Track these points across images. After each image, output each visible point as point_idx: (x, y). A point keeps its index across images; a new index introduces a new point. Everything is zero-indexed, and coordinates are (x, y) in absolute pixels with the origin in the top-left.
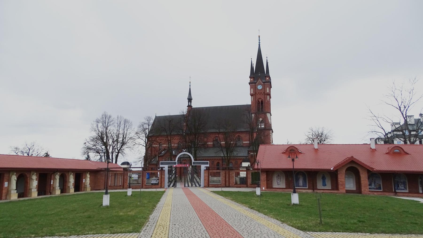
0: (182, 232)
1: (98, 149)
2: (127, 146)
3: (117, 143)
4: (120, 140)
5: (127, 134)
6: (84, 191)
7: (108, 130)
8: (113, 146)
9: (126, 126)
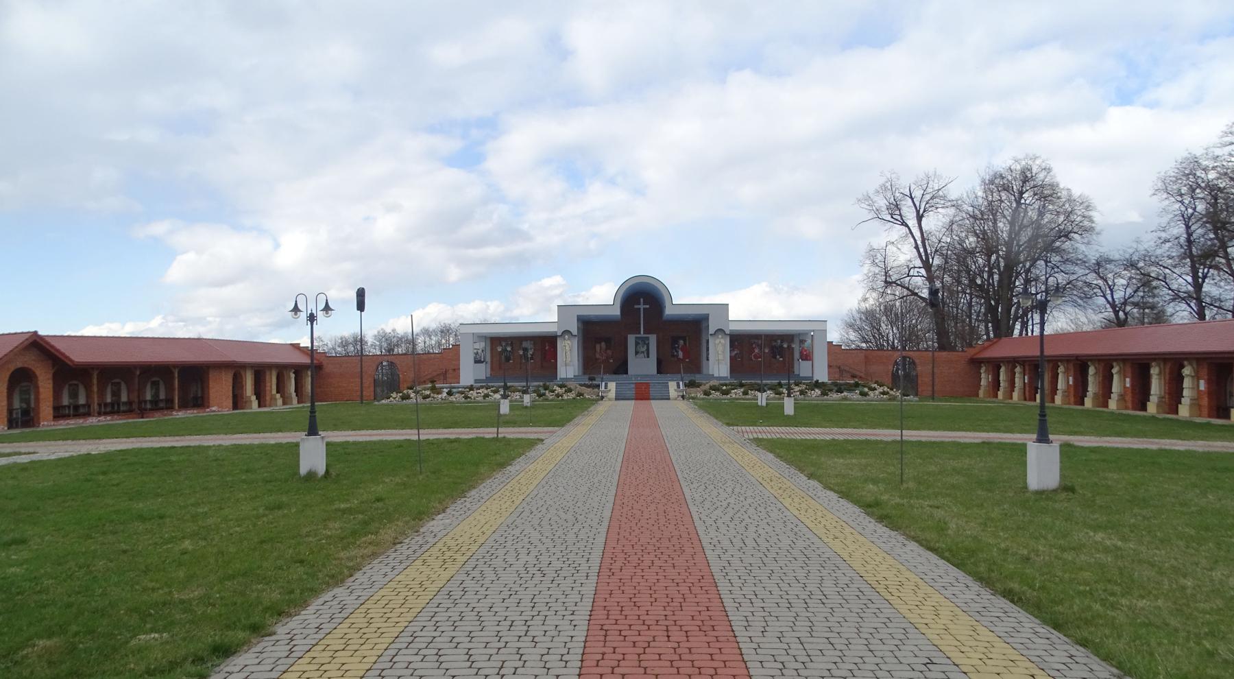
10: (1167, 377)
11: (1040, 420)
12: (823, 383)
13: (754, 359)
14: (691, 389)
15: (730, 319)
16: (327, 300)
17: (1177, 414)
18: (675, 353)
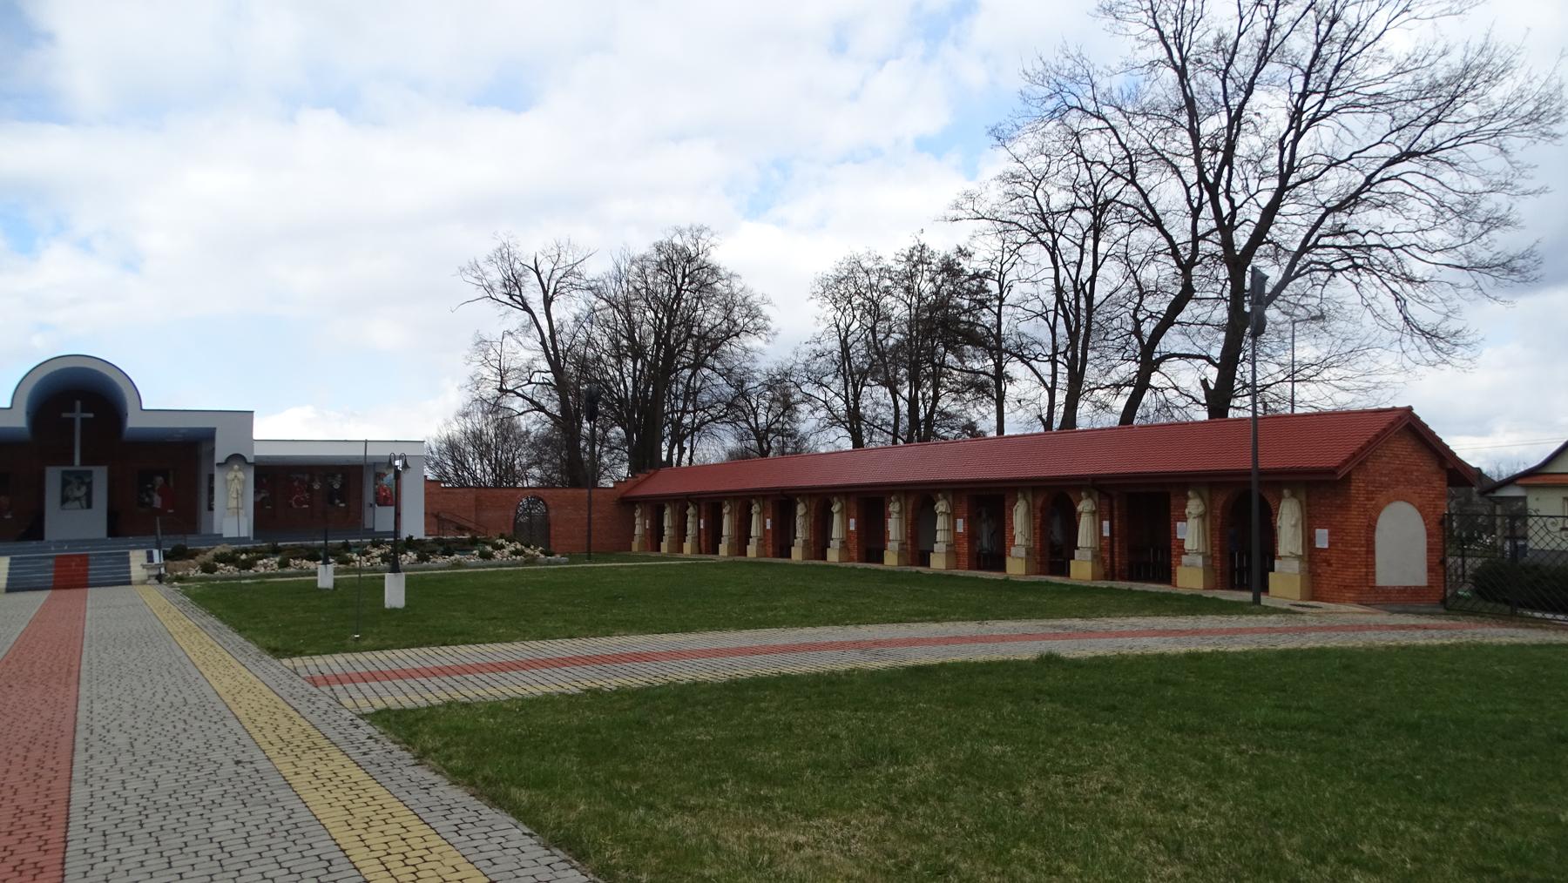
0: (187, 735)
10: (910, 517)
12: (419, 540)
13: (295, 506)
14: (177, 562)
15: (255, 437)
17: (746, 555)
18: (147, 500)
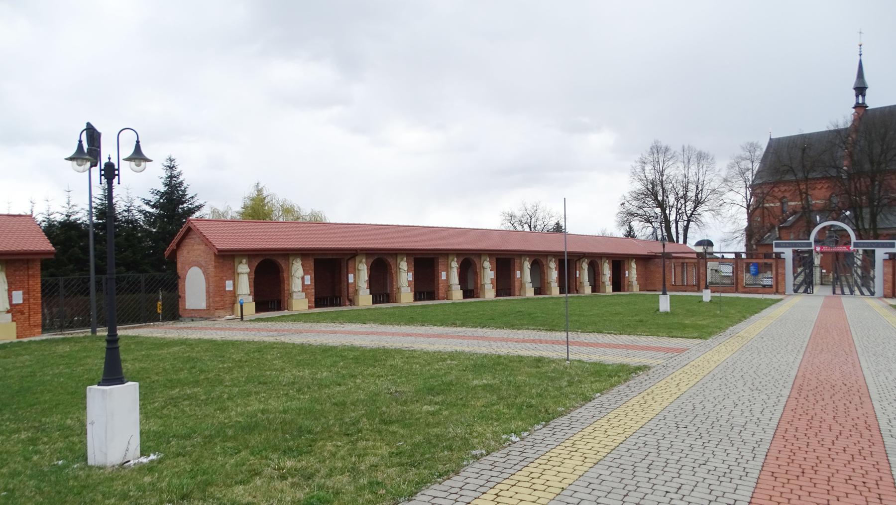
1: (648, 215)
2: (706, 208)
3: (686, 202)
4: (691, 194)
5: (705, 182)
6: (628, 290)
7: (665, 177)
8: (677, 208)
9: (701, 166)
11: (108, 349)
16: (138, 142)
